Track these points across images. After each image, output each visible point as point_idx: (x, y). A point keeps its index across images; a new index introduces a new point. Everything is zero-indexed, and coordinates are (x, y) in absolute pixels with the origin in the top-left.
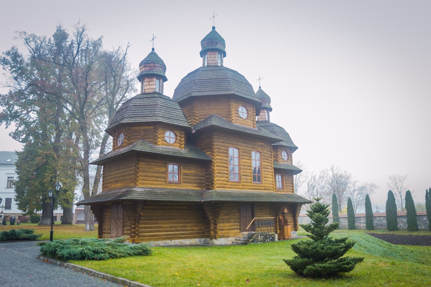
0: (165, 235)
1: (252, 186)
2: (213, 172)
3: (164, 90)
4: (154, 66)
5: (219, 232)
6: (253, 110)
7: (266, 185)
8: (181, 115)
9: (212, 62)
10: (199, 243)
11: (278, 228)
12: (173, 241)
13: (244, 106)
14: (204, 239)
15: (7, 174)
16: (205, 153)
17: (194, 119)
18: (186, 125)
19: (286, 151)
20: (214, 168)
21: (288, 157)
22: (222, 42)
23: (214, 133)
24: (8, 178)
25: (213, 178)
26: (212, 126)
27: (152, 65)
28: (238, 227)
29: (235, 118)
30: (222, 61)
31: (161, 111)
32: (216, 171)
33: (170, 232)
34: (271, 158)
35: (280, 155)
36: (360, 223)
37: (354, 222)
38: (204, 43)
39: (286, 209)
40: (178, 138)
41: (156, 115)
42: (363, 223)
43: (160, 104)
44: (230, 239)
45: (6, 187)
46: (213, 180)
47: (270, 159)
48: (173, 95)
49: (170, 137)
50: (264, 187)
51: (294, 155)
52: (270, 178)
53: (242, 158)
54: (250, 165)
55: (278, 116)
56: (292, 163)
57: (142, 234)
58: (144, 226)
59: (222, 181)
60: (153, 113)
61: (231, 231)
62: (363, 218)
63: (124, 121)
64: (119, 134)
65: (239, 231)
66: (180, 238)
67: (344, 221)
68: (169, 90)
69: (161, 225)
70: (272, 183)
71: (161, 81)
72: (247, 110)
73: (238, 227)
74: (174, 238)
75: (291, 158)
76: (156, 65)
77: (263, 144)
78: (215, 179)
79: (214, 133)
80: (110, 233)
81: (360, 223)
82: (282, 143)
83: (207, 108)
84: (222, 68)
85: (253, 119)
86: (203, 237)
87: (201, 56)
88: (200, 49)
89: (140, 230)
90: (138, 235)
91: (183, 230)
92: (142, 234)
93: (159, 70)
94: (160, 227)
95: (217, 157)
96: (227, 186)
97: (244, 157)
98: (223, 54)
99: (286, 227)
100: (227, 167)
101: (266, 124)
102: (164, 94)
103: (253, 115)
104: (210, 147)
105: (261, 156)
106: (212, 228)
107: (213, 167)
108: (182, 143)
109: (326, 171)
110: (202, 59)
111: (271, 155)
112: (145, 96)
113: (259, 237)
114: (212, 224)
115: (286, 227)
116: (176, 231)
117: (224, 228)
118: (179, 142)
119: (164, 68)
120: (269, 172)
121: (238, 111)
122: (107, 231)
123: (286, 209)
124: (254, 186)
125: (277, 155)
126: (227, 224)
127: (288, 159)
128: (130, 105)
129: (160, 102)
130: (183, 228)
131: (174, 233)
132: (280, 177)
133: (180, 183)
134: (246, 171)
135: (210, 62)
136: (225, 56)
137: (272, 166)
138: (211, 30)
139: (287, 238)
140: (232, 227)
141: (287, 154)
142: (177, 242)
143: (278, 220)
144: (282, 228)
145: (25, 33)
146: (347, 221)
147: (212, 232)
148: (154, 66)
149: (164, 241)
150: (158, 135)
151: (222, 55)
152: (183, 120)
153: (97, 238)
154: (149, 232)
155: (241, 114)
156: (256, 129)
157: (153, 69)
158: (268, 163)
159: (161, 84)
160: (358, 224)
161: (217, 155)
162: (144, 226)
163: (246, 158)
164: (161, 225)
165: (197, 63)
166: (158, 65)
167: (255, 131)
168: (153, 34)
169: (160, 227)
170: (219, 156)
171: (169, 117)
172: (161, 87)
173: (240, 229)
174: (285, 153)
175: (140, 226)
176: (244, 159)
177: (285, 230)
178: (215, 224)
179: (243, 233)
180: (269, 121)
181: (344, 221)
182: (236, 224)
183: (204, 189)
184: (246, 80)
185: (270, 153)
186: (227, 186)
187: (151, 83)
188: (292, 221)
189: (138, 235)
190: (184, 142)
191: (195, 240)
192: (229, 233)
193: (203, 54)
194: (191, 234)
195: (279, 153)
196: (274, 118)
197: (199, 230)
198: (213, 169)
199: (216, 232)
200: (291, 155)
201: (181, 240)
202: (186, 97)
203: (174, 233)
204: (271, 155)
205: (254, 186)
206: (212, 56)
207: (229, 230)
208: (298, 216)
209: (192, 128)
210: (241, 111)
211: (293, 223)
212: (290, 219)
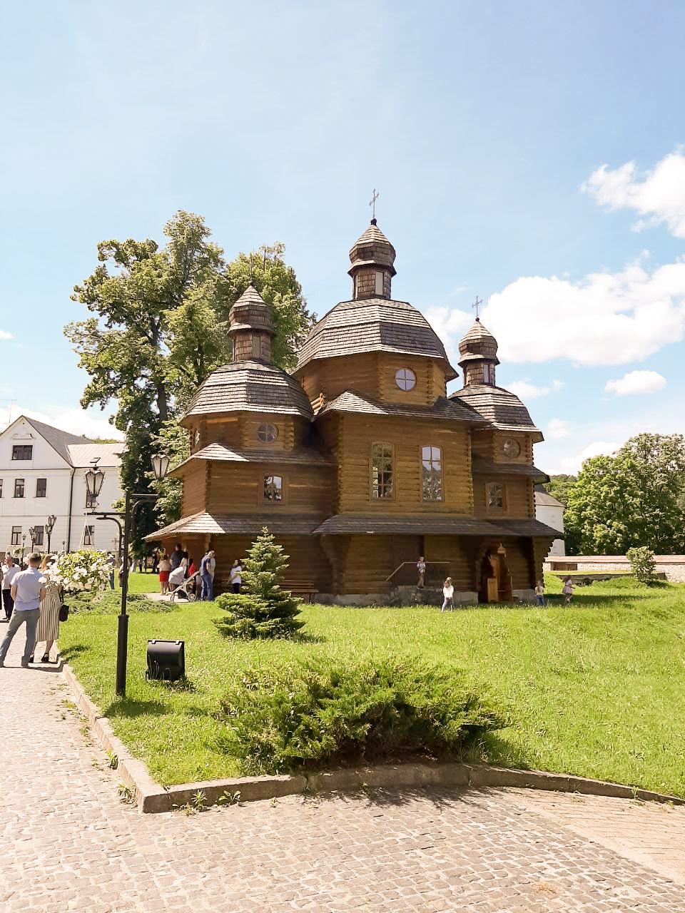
2: (340, 486)
4: (248, 315)
5: (348, 585)
13: (408, 368)
24: (14, 447)
29: (388, 391)
39: (501, 547)
45: (85, 506)
46: (339, 498)
51: (537, 448)
72: (415, 373)
78: (343, 496)
79: (341, 421)
95: (348, 460)
105: (443, 454)
106: (335, 577)
107: (339, 478)
123: (501, 547)
150: (244, 431)
158: (459, 464)
161: (347, 458)
170: (351, 458)
198: (340, 480)
206: (368, 271)
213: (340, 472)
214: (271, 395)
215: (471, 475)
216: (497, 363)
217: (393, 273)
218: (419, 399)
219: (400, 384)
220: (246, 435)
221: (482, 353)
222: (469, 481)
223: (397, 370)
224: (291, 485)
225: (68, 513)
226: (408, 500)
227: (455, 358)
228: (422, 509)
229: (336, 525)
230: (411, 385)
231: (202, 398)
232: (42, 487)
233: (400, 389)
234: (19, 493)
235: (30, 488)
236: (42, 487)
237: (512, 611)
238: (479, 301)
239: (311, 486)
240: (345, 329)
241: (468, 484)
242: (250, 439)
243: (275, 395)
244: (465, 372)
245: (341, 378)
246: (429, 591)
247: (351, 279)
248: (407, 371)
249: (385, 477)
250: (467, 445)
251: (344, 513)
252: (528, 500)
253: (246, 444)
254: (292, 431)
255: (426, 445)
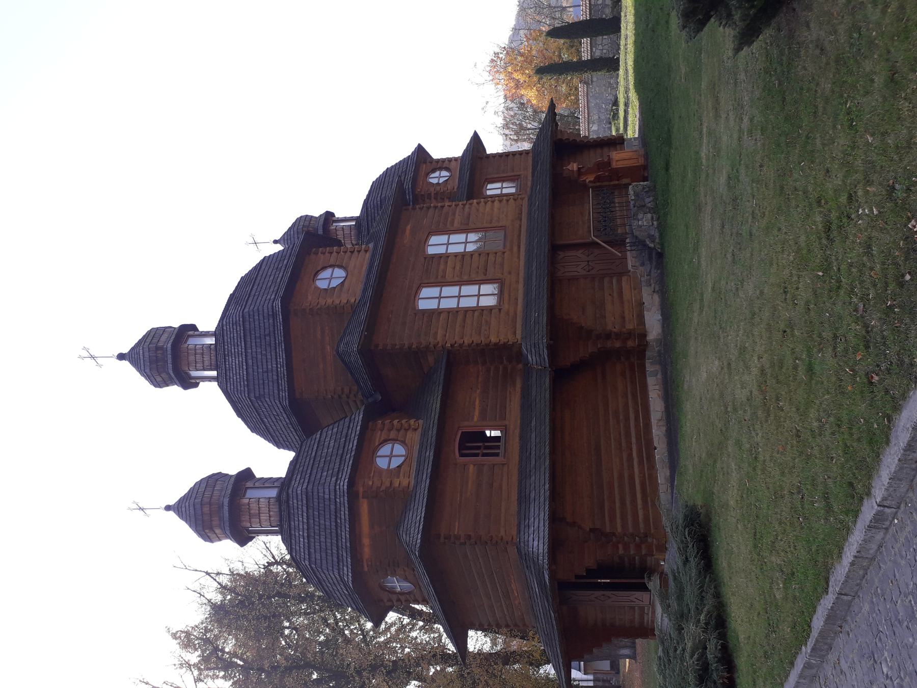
0: (641, 462)
2: (477, 345)
3: (275, 475)
5: (629, 326)
6: (324, 253)
8: (335, 430)
9: (206, 358)
10: (659, 376)
11: (617, 182)
14: (648, 365)
17: (348, 397)
18: (359, 417)
19: (427, 174)
20: (466, 343)
21: (441, 169)
22: (154, 335)
23: (380, 347)
26: (361, 352)
27: (206, 509)
28: (614, 281)
30: (206, 334)
31: (323, 481)
32: (476, 339)
33: (631, 449)
34: (442, 207)
35: (438, 188)
38: (159, 379)
40: (393, 434)
41: (332, 493)
43: (305, 484)
48: (287, 451)
49: (391, 456)
51: (437, 153)
52: (492, 210)
53: (444, 276)
54: (459, 257)
55: (346, 198)
56: (456, 159)
57: (642, 525)
58: (619, 521)
60: (327, 503)
63: (348, 578)
64: (383, 588)
65: (624, 279)
66: (648, 425)
67: (600, 47)
68: (272, 461)
69: (616, 475)
71: (249, 484)
73: (614, 281)
75: (443, 160)
76: (206, 500)
77: (409, 227)
78: (494, 339)
79: (380, 347)
80: (642, 609)
82: (408, 185)
83: (321, 366)
84: (219, 333)
85: (349, 254)
86: (643, 366)
87: (196, 385)
89: (631, 530)
90: (646, 536)
91: (627, 419)
92: (642, 525)
93: (221, 490)
94: (621, 476)
97: (440, 273)
98: (188, 330)
99: (614, 165)
101: (364, 224)
102: (284, 476)
103: (338, 253)
104: (416, 355)
106: (618, 344)
108: (406, 426)
110: (201, 384)
111: (436, 207)
112: (286, 526)
113: (640, 223)
114: (609, 344)
115: (614, 165)
116: (628, 435)
118: (402, 432)
119: (217, 478)
122: (637, 616)
123: (570, 167)
125: (436, 194)
127: (447, 169)
128: (307, 563)
129: (298, 488)
131: (634, 440)
132: (489, 186)
133: (506, 426)
135: (207, 363)
136: (193, 327)
137: (464, 205)
138: (126, 364)
139: (641, 161)
140: (615, 294)
141: (434, 171)
142: (658, 433)
143: (598, 184)
144: (617, 174)
147: (630, 344)
148: (210, 504)
149: (658, 466)
150: (383, 488)
151: (191, 333)
152: (347, 424)
153: (652, 642)
154: (636, 507)
155: (335, 283)
156: (371, 245)
157: (217, 507)
158: (454, 214)
159: (257, 485)
161: (436, 339)
162: (619, 521)
163: (442, 267)
164: (616, 475)
165: (209, 396)
166: (207, 494)
167: (375, 247)
168: (129, 509)
169: (621, 476)
170: (436, 333)
171: (338, 460)
172: (268, 483)
173: (620, 275)
174: (433, 175)
175: (619, 530)
176: (444, 271)
177: (620, 165)
178: (608, 336)
179: (630, 267)
180: (356, 219)
181: (600, 47)
182: (606, 284)
183: (520, 366)
184: (250, 271)
185: (431, 210)
187: (254, 511)
188: (599, 151)
189: (646, 536)
190: (404, 421)
191: (650, 388)
193: (188, 383)
194: (634, 396)
195: (432, 189)
196: (349, 205)
199: (630, 334)
200: (438, 161)
201: (654, 421)
202: (294, 419)
203: (634, 440)
206: (192, 358)
207: (622, 303)
208: (587, 137)
209: (370, 400)
210: (328, 281)
211: (606, 150)
212: (593, 158)
214: (330, 450)
215: (471, 201)
217: (247, 474)
218: (362, 261)
219: (396, 462)
220: (391, 484)
222: (478, 203)
224: (476, 419)
226: (502, 265)
228: (515, 249)
229: (537, 356)
230: (399, 449)
233: (343, 283)
239: (478, 391)
241: (482, 203)
242: (398, 477)
243: (332, 444)
245: (321, 366)
248: (379, 453)
250: (429, 208)
251: (519, 336)
253: (405, 483)
255: (424, 251)
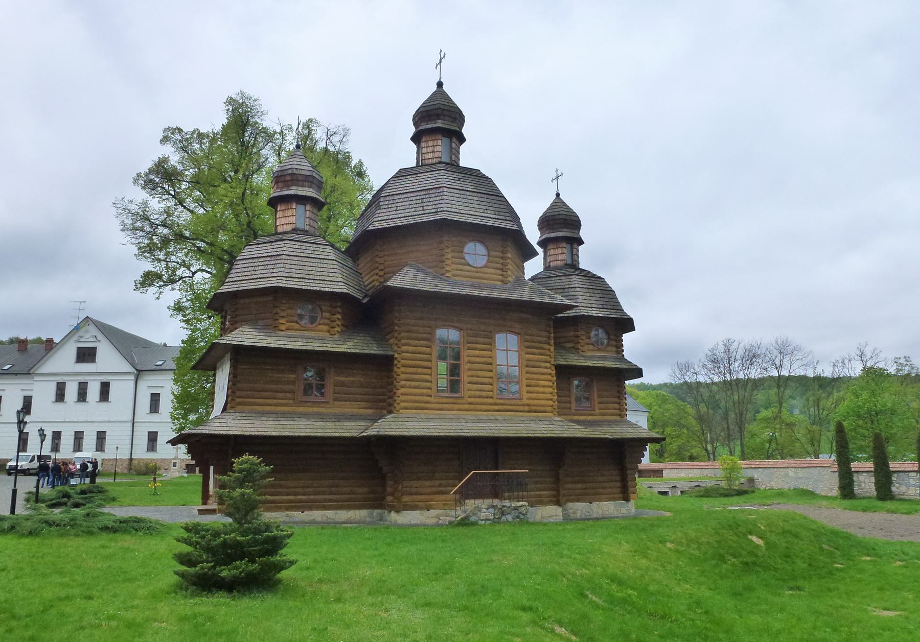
0: (291, 501)
1: (496, 404)
7: (531, 402)
9: (430, 156)
12: (306, 513)
15: (23, 390)
16: (388, 340)
25: (394, 390)
36: (908, 486)
37: (890, 483)
42: (915, 486)
44: (433, 512)
47: (546, 346)
50: (528, 405)
54: (489, 360)
59: (415, 395)
61: (436, 497)
62: (914, 474)
70: (549, 396)
74: (310, 508)
78: (398, 392)
81: (908, 486)
88: (412, 130)
91: (331, 493)
96: (428, 405)
100: (430, 368)
109: (846, 362)
111: (549, 338)
117: (420, 490)
120: (544, 374)
121: (462, 252)
124: (501, 404)
126: (428, 483)
130: (334, 489)
134: (481, 373)
138: (435, 88)
145: (180, 130)
146: (873, 479)
160: (903, 489)
186: (428, 405)
188: (618, 478)
192: (432, 500)
193: (416, 139)
197: (370, 493)
204: (549, 338)
205: (501, 404)
206: (431, 143)
213: (396, 362)
216: (581, 242)
221: (562, 225)
223: (465, 243)
225: (130, 419)
227: (533, 235)
231: (234, 275)
232: (105, 390)
234: (82, 396)
235: (94, 391)
236: (105, 390)
237: (714, 337)
238: (559, 174)
240: (404, 196)
244: (545, 253)
246: (504, 506)
247: (414, 147)
249: (454, 370)
252: (619, 397)
254: (339, 313)
255: (500, 332)
